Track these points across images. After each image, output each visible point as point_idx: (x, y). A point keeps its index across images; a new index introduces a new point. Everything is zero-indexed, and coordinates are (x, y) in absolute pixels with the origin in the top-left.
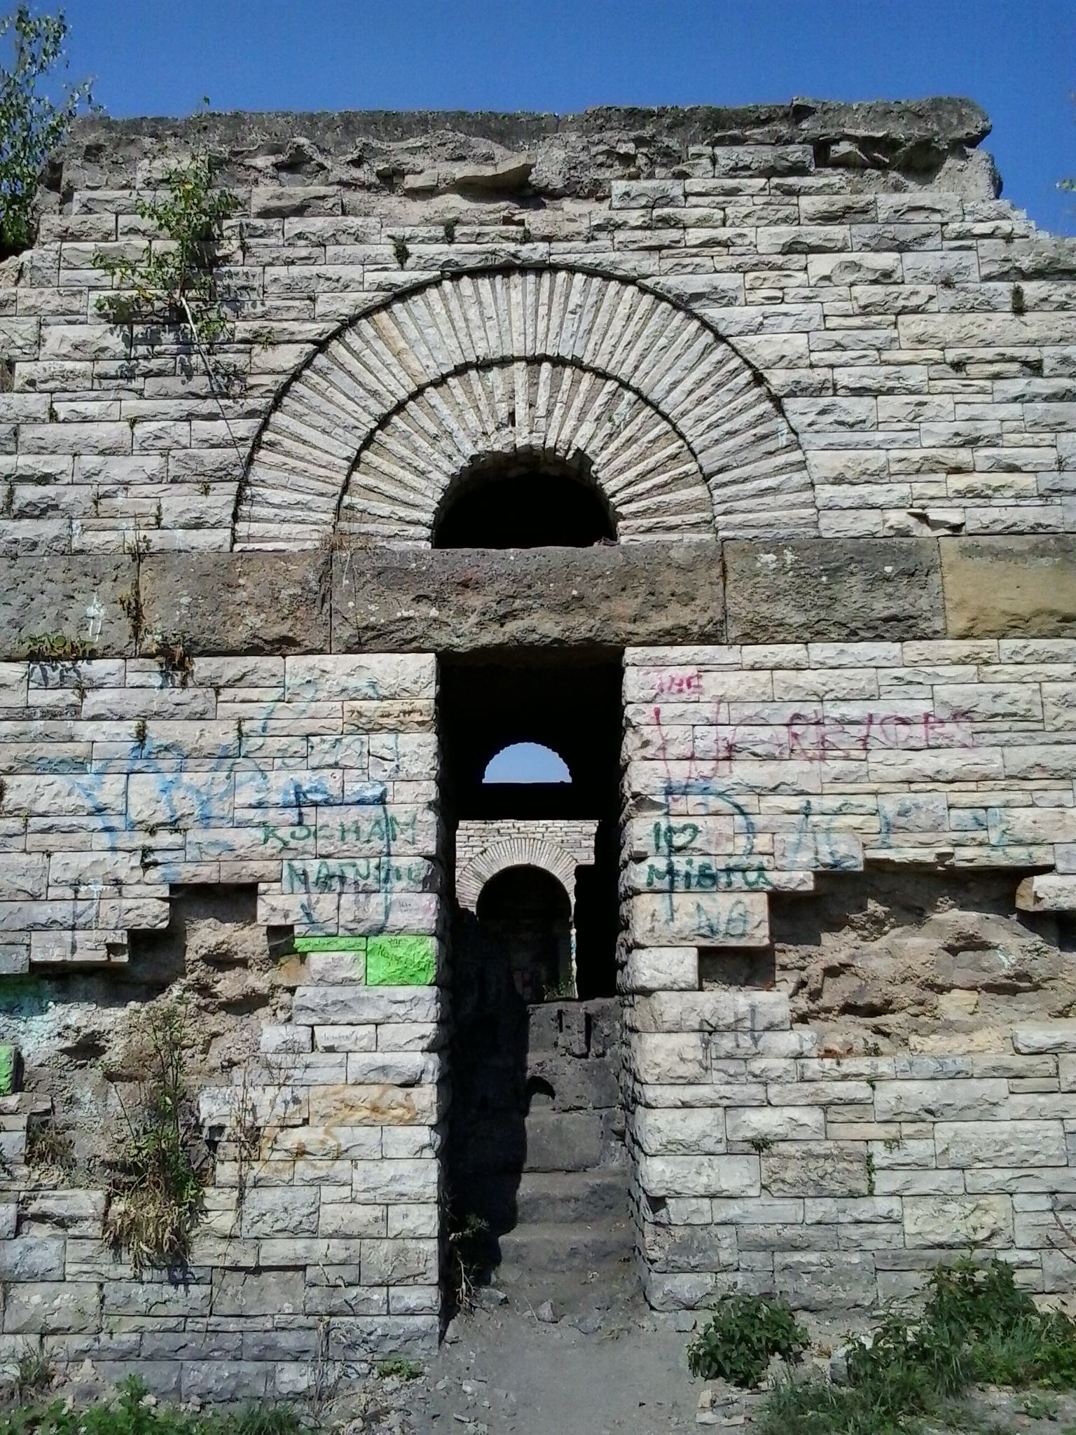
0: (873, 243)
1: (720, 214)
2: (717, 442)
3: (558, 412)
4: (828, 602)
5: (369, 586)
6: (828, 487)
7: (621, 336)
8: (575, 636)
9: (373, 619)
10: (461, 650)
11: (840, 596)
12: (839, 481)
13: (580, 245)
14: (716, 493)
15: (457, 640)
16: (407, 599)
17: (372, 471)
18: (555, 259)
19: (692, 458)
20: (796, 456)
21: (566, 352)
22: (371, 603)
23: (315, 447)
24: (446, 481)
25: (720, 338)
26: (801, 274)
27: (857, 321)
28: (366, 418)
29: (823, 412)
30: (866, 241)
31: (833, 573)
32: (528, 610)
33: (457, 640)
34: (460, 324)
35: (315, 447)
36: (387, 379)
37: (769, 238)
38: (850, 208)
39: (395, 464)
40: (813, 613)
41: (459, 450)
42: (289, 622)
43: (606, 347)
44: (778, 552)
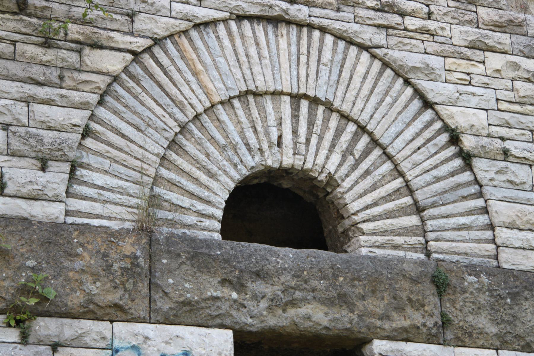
0: (526, 51)
1: (426, 10)
2: (429, 184)
3: (314, 140)
4: (511, 319)
5: (184, 267)
6: (505, 230)
7: (359, 91)
8: (340, 326)
9: (189, 295)
10: (251, 329)
11: (519, 315)
12: (511, 227)
13: (332, 14)
14: (429, 223)
15: (250, 321)
16: (215, 281)
17: (174, 168)
18: (316, 21)
19: (407, 192)
20: (480, 202)
21: (321, 95)
22: (188, 281)
23: (132, 141)
24: (232, 186)
25: (427, 104)
26: (481, 65)
27: (517, 108)
28: (171, 123)
29: (499, 172)
30: (522, 48)
31: (514, 296)
32: (304, 300)
33: (250, 321)
34: (243, 58)
35: (132, 141)
36: (187, 91)
37: (460, 35)
38: (511, 21)
39: (194, 165)
40: (503, 326)
41: (242, 161)
42: (120, 292)
43: (350, 96)
44: (477, 275)
